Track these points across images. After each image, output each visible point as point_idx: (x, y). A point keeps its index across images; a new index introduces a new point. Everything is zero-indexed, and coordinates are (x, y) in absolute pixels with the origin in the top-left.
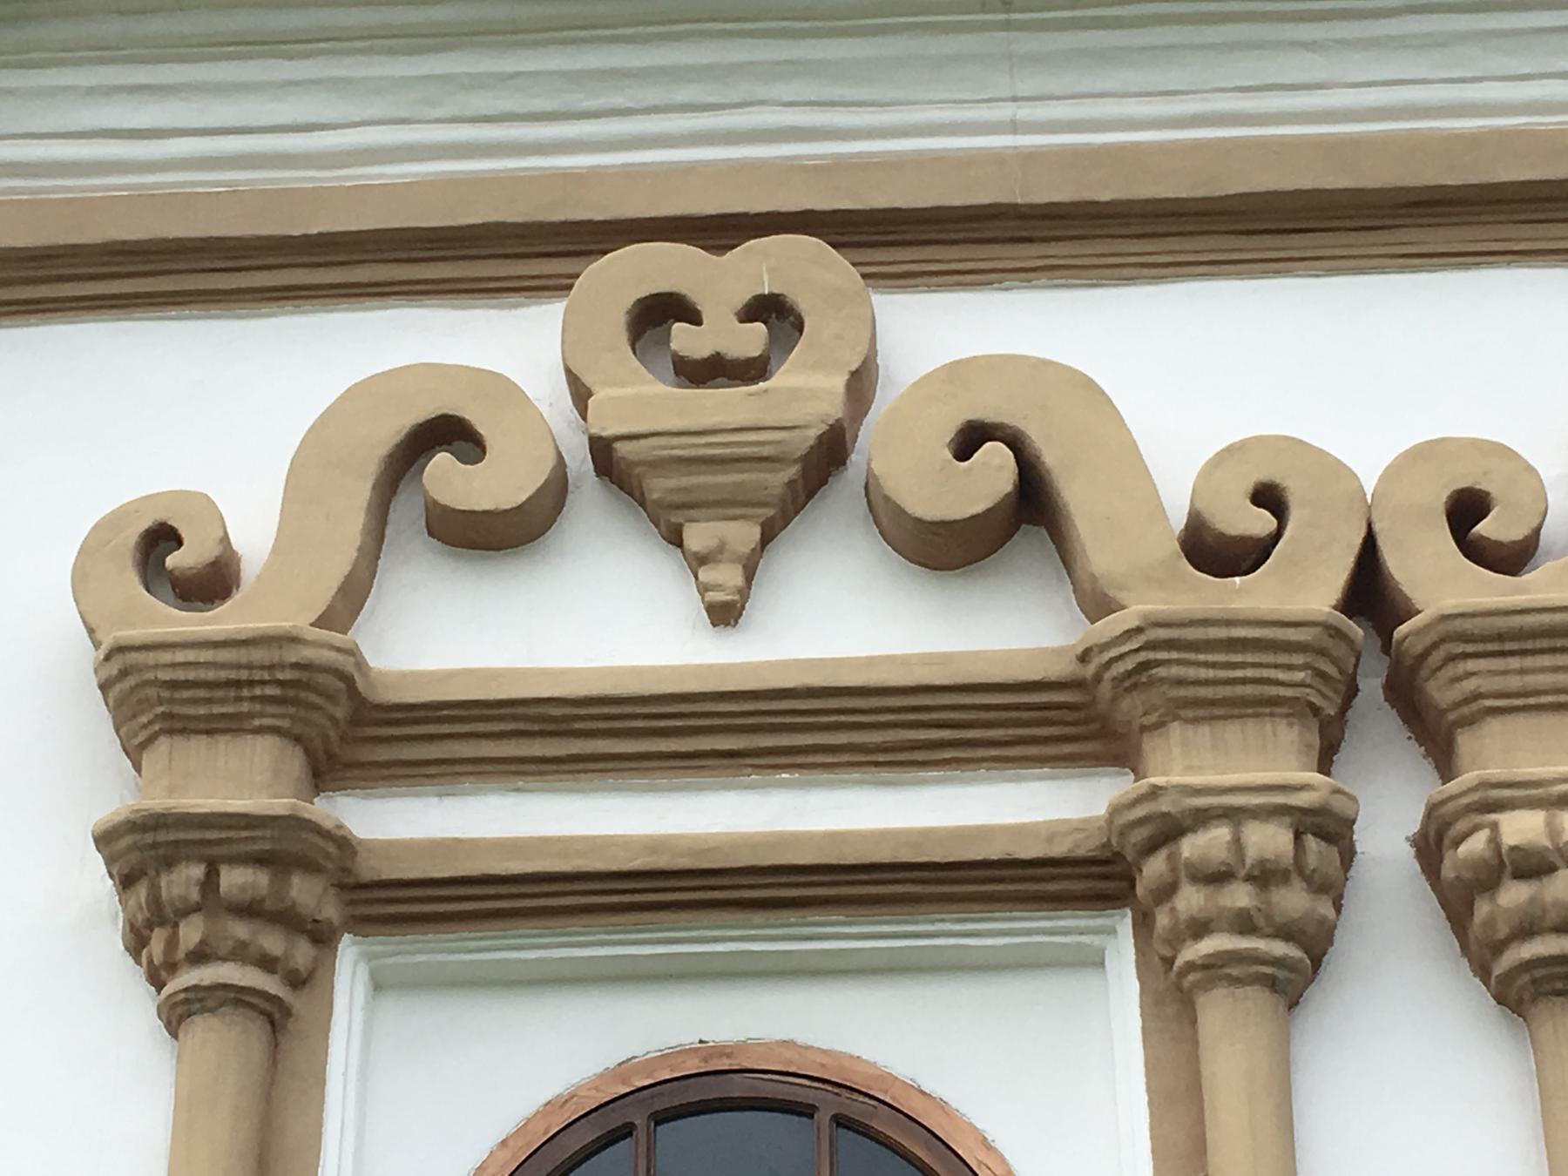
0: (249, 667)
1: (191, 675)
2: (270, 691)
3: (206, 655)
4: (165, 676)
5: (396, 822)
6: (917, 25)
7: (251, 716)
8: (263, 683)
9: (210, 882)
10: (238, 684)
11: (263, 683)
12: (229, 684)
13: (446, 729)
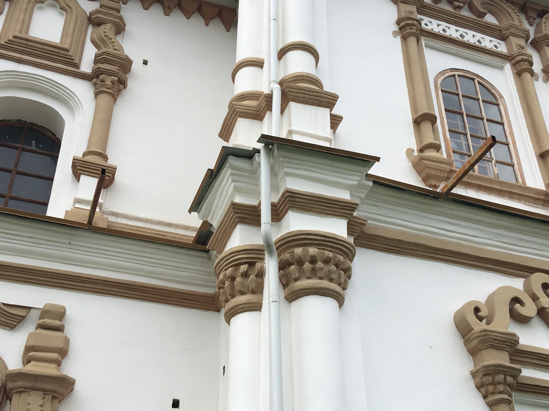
0: (507, 339)
1: (498, 338)
2: (510, 344)
3: (500, 335)
4: (494, 337)
5: (529, 373)
6: (511, 195)
7: (505, 348)
8: (508, 342)
9: (505, 379)
10: (504, 341)
11: (508, 342)
12: (502, 341)
13: (526, 356)
